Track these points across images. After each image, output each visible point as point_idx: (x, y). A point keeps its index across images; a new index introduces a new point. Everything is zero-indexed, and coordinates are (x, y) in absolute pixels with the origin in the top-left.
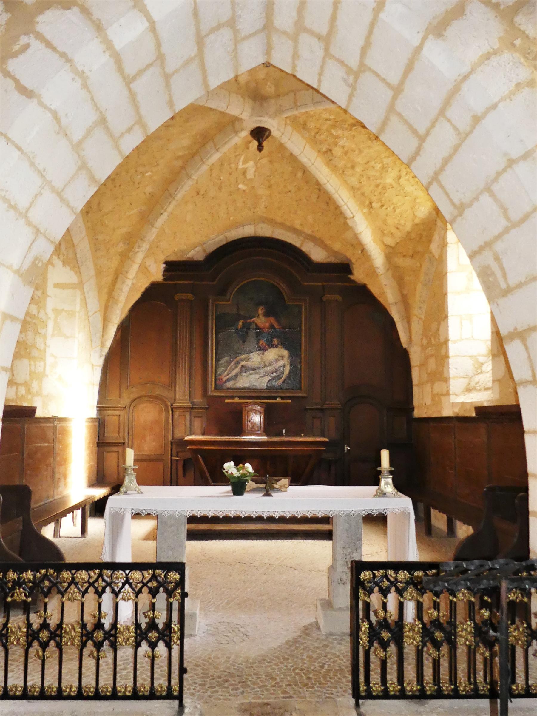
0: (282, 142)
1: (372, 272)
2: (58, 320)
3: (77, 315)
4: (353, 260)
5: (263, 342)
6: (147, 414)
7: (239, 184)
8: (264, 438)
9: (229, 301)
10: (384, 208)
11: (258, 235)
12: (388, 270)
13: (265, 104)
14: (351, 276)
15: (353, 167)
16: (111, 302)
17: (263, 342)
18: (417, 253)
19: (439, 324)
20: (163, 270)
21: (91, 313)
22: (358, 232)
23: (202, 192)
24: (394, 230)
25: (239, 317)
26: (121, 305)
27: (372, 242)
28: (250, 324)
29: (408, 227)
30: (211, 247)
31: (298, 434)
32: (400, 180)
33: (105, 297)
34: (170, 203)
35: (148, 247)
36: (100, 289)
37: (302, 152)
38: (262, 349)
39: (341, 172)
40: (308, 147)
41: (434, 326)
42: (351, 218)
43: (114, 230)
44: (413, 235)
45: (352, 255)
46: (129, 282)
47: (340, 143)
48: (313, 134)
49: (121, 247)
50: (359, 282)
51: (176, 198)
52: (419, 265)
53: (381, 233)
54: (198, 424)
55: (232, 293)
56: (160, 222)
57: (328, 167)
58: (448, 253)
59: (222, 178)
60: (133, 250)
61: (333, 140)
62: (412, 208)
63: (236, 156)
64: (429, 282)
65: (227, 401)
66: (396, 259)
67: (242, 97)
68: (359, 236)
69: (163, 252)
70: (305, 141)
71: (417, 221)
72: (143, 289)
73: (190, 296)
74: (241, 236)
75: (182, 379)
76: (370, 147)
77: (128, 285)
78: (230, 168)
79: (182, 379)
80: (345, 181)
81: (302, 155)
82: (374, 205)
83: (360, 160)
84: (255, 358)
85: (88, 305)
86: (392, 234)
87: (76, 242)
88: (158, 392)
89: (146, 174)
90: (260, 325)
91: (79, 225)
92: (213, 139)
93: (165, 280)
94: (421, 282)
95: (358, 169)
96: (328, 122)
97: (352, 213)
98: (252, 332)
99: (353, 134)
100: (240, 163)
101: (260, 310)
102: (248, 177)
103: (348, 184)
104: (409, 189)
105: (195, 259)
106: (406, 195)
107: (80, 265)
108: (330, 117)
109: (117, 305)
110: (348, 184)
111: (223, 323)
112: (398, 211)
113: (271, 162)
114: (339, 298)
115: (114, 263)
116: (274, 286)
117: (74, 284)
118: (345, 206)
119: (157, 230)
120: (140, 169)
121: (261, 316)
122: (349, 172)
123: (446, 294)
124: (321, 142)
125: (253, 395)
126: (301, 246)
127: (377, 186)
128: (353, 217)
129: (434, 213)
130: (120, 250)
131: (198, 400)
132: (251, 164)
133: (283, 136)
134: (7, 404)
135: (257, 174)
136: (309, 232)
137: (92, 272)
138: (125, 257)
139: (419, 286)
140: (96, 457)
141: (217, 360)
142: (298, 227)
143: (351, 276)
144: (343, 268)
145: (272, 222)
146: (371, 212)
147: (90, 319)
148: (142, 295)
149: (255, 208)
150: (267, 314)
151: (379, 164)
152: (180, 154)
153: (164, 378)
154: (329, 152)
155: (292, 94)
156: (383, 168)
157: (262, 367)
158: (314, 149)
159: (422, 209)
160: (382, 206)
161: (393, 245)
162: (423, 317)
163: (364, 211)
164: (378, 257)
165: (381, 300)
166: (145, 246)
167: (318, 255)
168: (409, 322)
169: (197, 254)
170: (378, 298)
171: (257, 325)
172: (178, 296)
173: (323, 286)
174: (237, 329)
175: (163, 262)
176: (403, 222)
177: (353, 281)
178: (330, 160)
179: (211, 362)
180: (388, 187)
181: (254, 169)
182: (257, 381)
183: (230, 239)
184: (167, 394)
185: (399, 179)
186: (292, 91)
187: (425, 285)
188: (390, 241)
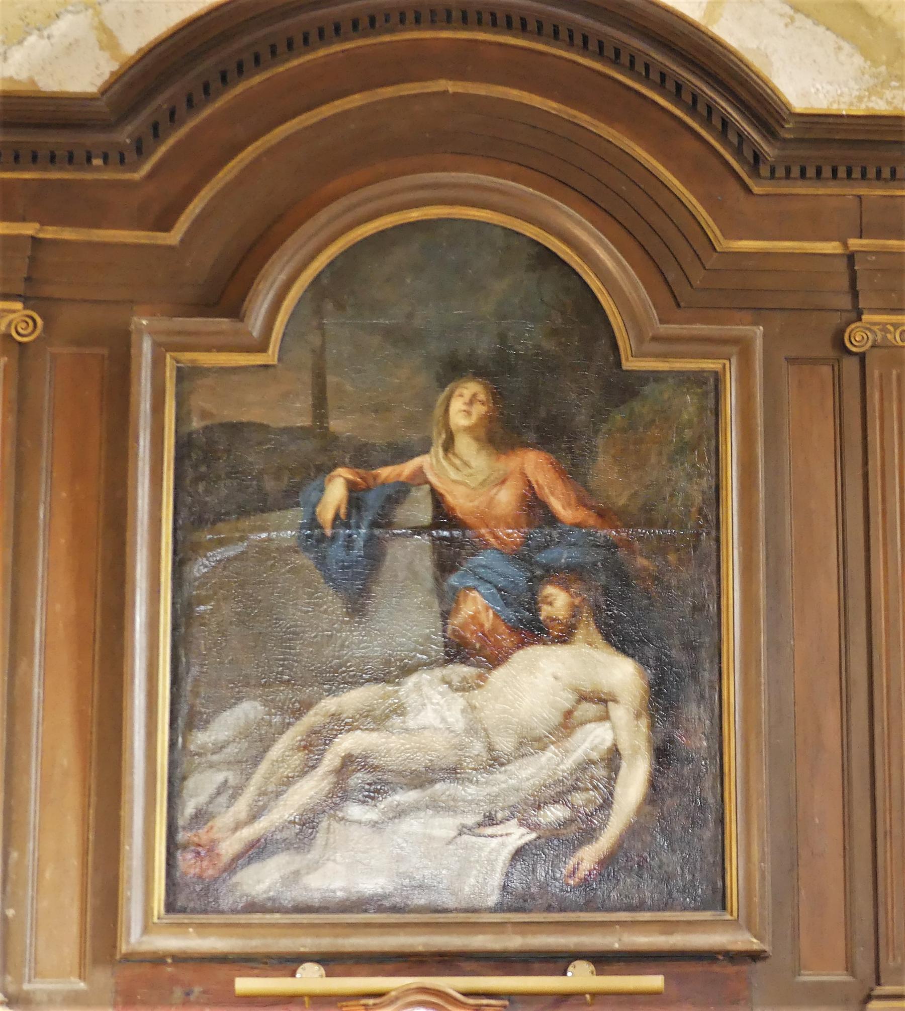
9: (262, 347)
25: (323, 451)
28: (399, 493)
55: (279, 294)
90: (460, 500)
101: (457, 405)
116: (546, 258)
121: (465, 445)
150: (501, 435)
171: (437, 499)
173: (851, 258)
174: (314, 523)
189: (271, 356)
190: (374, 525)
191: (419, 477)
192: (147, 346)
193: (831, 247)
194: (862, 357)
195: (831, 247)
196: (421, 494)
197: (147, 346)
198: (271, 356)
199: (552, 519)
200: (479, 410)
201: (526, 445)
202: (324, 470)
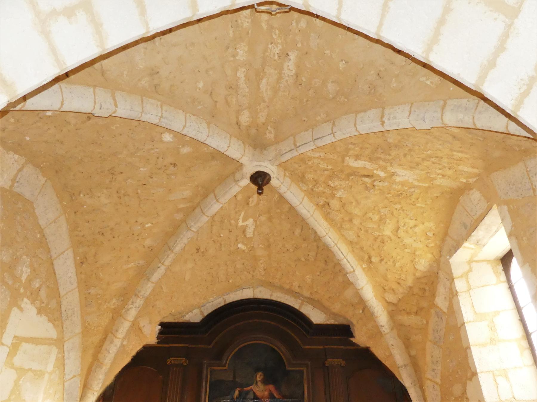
0: (281, 191)
1: (377, 333)
2: (21, 382)
3: (47, 376)
4: (355, 322)
7: (239, 243)
9: (225, 366)
10: (383, 262)
11: (256, 297)
12: (392, 329)
13: (265, 152)
14: (352, 339)
15: (351, 220)
16: (96, 364)
18: (422, 309)
19: (464, 385)
20: (158, 332)
21: (67, 377)
22: (359, 288)
23: (202, 250)
24: (395, 286)
25: (235, 385)
26: (105, 368)
27: (374, 298)
28: (248, 393)
29: (410, 282)
30: (208, 310)
32: (399, 231)
33: (89, 359)
34: (168, 256)
35: (142, 302)
36: (84, 351)
37: (301, 203)
39: (339, 225)
40: (306, 200)
41: (457, 389)
42: (351, 272)
43: (108, 284)
44: (416, 290)
45: (353, 317)
46: (118, 342)
47: (338, 195)
48: (311, 186)
49: (114, 303)
50: (362, 346)
51: (174, 251)
52: (425, 322)
53: (382, 289)
55: (228, 358)
56: (156, 276)
57: (327, 221)
58: (460, 302)
59: (222, 235)
60: (126, 306)
61: (330, 192)
62: (412, 261)
63: (236, 213)
64: (440, 339)
66: (400, 317)
67: (243, 143)
68: (360, 292)
69: (159, 312)
70: (302, 194)
71: (418, 274)
72: (134, 353)
73: (183, 361)
74: (240, 298)
76: (367, 198)
77: (116, 346)
78: (231, 225)
80: (343, 236)
81: (301, 206)
82: (373, 259)
83: (357, 211)
85: (66, 367)
86: (393, 290)
87: (62, 292)
89: (147, 226)
90: (258, 394)
91: (70, 275)
92: (213, 191)
93: (158, 343)
94: (431, 341)
95: (356, 222)
96: (326, 172)
97: (352, 267)
99: (350, 184)
100: (241, 221)
101: (258, 376)
102: (248, 236)
103: (346, 239)
104: (408, 241)
105: (192, 321)
106: (405, 246)
107: (64, 318)
108: (328, 167)
109: (101, 369)
110: (346, 239)
112: (398, 265)
113: (270, 219)
114: (343, 363)
115: (105, 320)
116: (273, 350)
117: (52, 339)
118: (345, 260)
119: (152, 285)
120: (141, 220)
121: (259, 383)
122: (347, 225)
123: (468, 347)
124: (319, 195)
126: (300, 307)
127: (375, 239)
128: (354, 271)
129: (435, 265)
130: (112, 307)
132: (251, 221)
133: (282, 186)
135: (256, 233)
136: (307, 294)
137: (78, 329)
138: (117, 314)
139: (429, 346)
142: (297, 290)
143: (352, 339)
144: (344, 331)
145: (270, 285)
146: (370, 268)
147: (66, 384)
148: (132, 359)
149: (254, 271)
150: (265, 382)
151: (377, 215)
152: (182, 206)
154: (327, 206)
155: (292, 138)
156: (381, 219)
158: (312, 202)
159: (423, 261)
160: (381, 260)
161: (395, 301)
162: (438, 380)
163: (364, 266)
164: (382, 317)
165: (387, 364)
166: (139, 302)
167: (317, 317)
168: (422, 388)
170: (384, 362)
171: (254, 393)
172: (170, 361)
173: (325, 349)
174: (233, 398)
175: (158, 323)
176: (403, 277)
177: (354, 344)
178: (328, 213)
180: (386, 239)
181: (253, 227)
183: (228, 301)
185: (397, 231)
186: (292, 135)
187: (435, 343)
188: (391, 298)
189: (226, 368)
190: (243, 399)
191: (251, 390)
192: (205, 366)
193: (322, 347)
194: (328, 367)
195: (322, 347)
196: (251, 393)
197: (205, 366)
198: (226, 368)
199: (275, 398)
200: (262, 377)
201: (270, 384)
202: (234, 389)
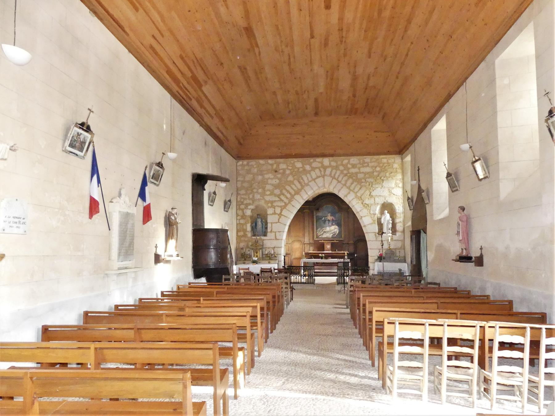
5: (330, 224)
6: (297, 245)
8: (331, 252)
17: (330, 224)
31: (341, 251)
38: (330, 226)
54: (311, 248)
65: (89, 314)
75: (307, 234)
79: (307, 234)
84: (328, 229)
88: (300, 239)
98: (327, 222)
111: (319, 219)
125: (328, 240)
131: (311, 241)
134: (533, 339)
140: (495, 50)
141: (317, 229)
150: (331, 216)
153: (301, 235)
157: (330, 230)
169: (311, 199)
179: (315, 231)
182: (329, 235)
184: (302, 239)
